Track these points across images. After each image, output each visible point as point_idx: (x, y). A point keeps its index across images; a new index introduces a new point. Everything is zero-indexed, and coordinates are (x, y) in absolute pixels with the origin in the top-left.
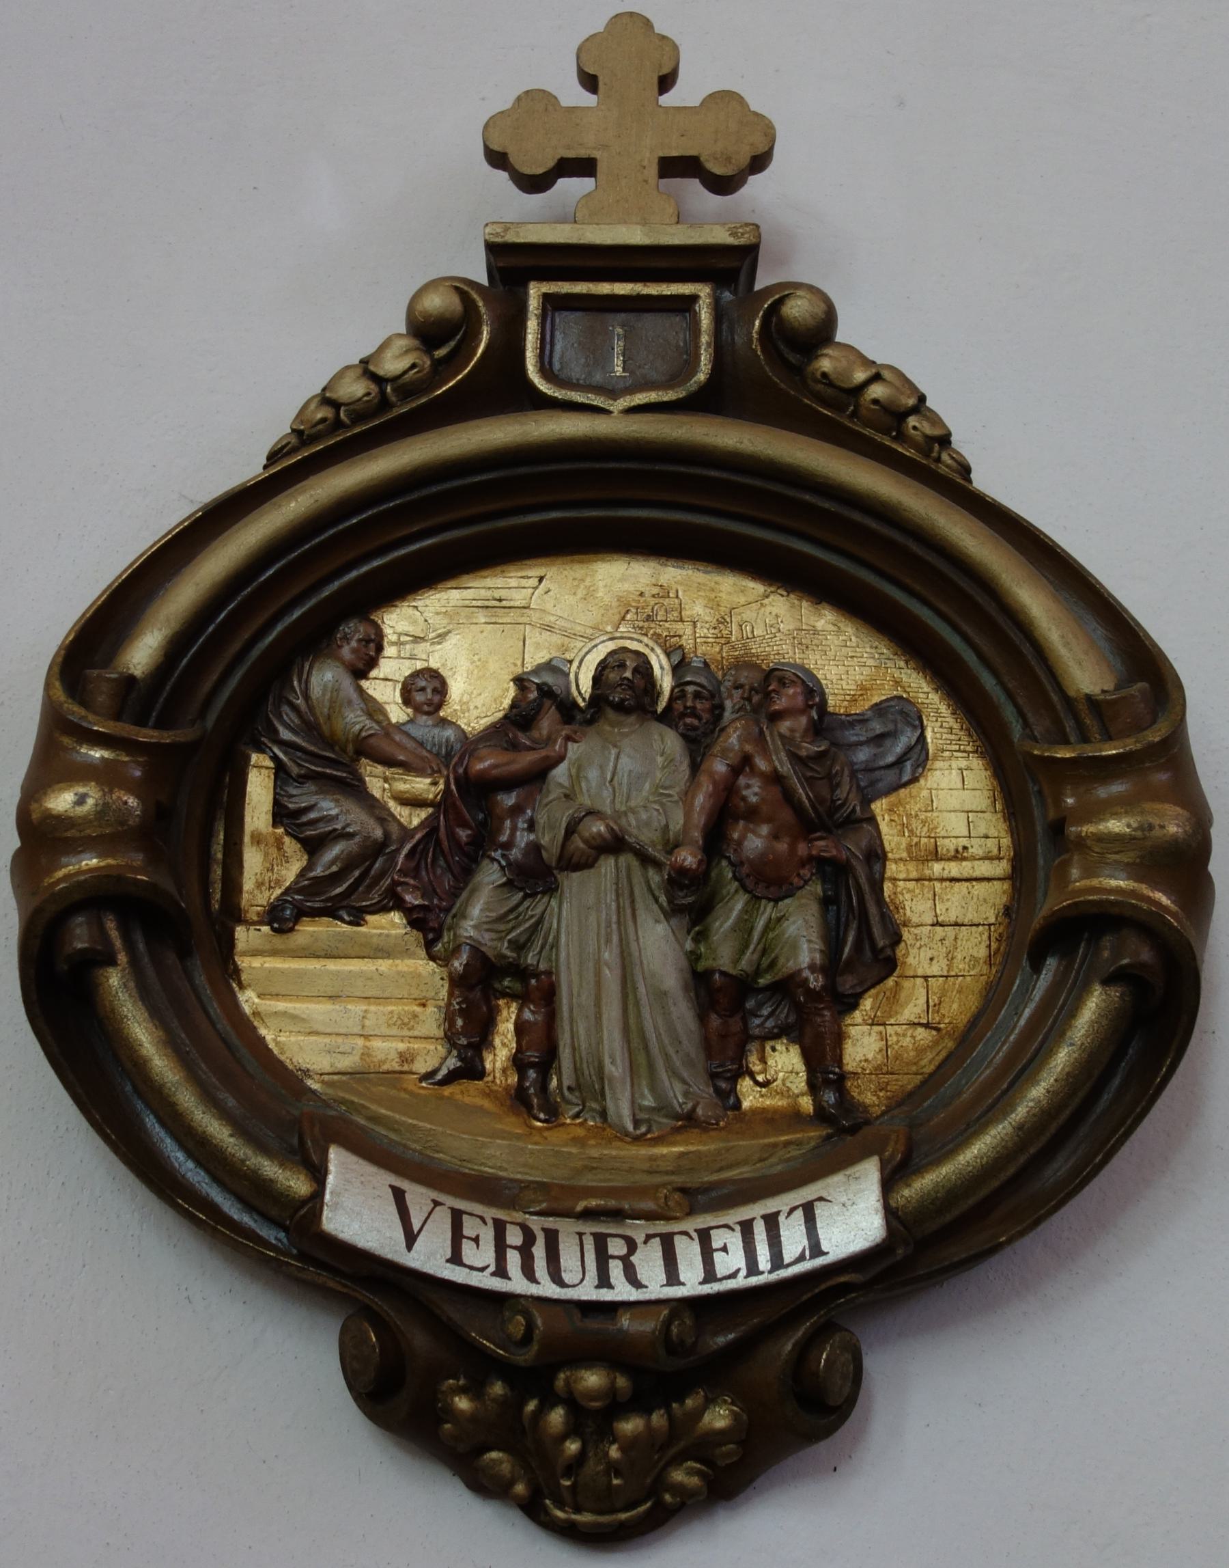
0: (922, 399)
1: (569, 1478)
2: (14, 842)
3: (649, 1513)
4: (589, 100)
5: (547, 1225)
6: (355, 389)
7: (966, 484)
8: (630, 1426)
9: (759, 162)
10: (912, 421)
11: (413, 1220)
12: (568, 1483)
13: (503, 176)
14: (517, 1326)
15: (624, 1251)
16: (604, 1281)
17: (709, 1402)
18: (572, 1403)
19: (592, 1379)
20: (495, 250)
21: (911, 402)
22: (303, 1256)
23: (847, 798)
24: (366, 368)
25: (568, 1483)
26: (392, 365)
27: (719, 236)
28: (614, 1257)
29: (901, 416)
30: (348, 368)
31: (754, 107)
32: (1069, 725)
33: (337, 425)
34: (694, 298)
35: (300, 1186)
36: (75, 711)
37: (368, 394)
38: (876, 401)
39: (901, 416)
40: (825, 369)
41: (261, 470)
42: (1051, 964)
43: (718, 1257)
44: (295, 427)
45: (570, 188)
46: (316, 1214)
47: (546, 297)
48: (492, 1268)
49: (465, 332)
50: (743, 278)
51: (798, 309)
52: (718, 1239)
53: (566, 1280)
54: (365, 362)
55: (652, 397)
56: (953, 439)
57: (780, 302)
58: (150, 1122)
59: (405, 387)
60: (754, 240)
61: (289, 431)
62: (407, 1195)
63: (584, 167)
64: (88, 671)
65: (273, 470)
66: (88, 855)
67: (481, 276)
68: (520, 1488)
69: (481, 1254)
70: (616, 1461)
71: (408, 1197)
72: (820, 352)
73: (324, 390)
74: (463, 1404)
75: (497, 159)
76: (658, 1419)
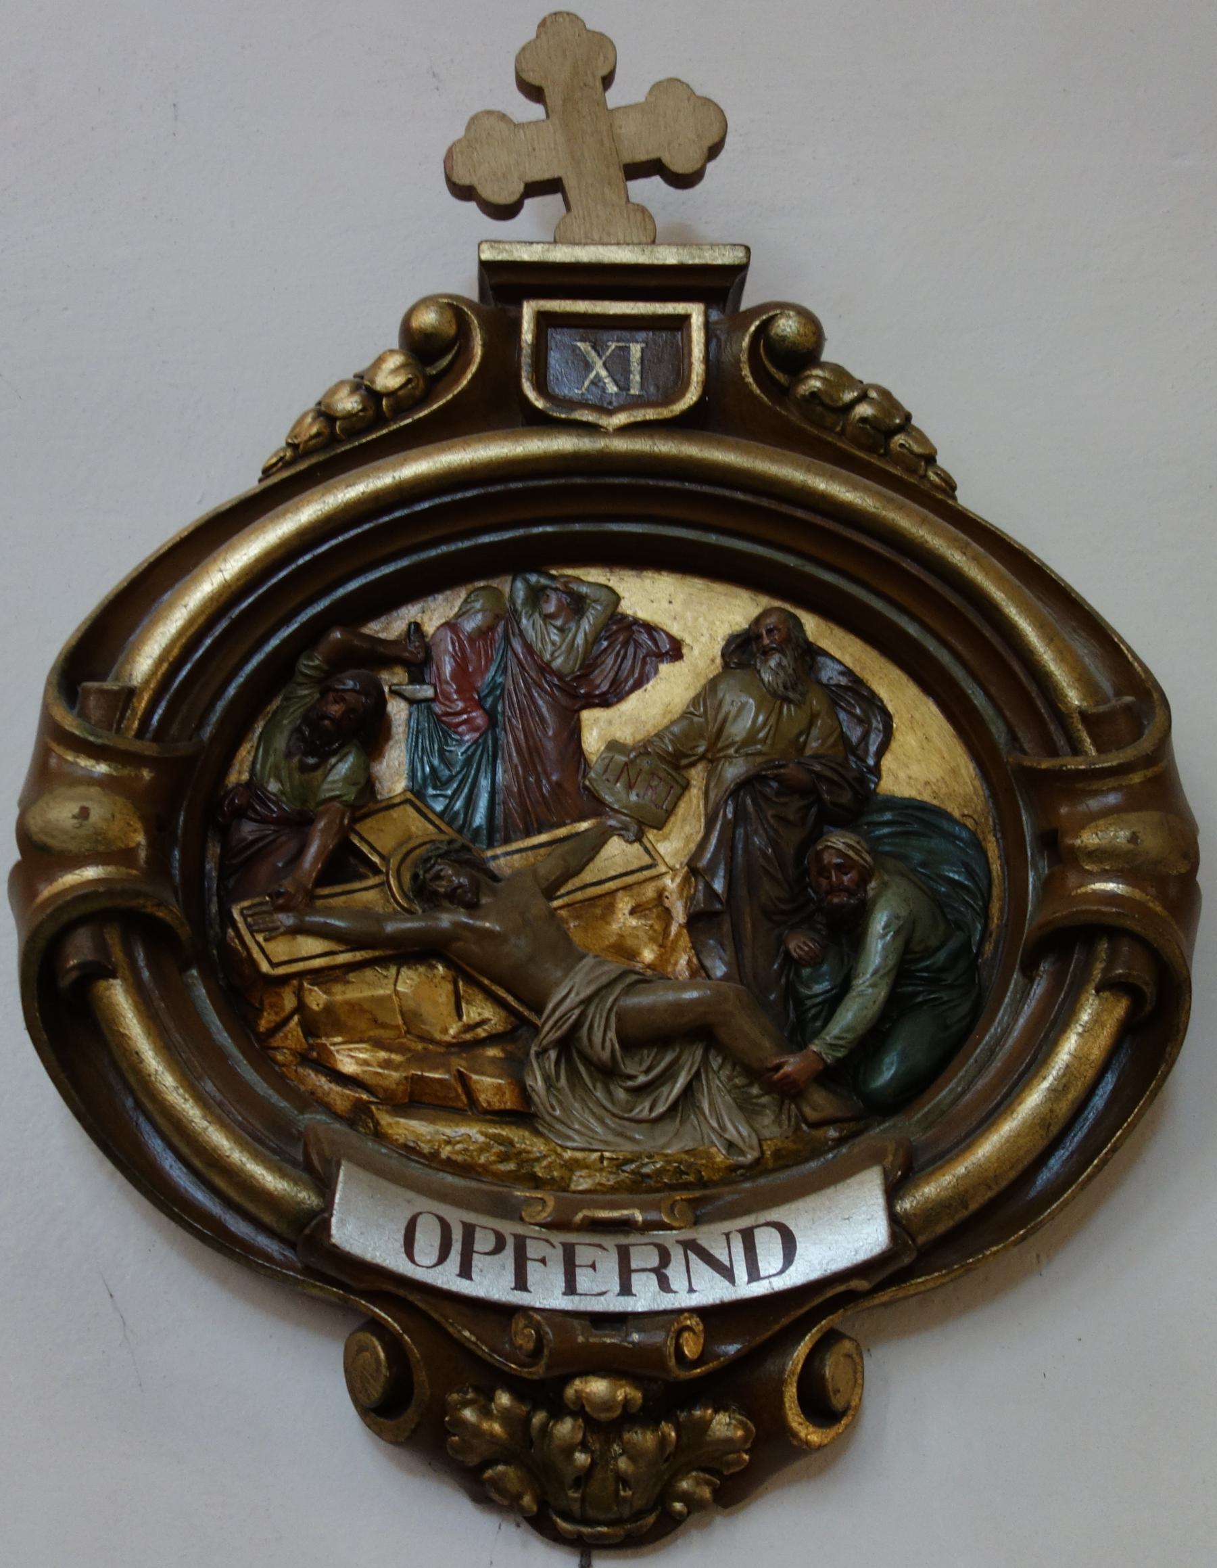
0: (908, 417)
2: (14, 855)
4: (535, 111)
6: (348, 403)
8: (644, 1439)
10: (900, 439)
14: (524, 1339)
15: (655, 1262)
17: (716, 1411)
18: (580, 1409)
19: (598, 1387)
20: (488, 268)
22: (308, 1271)
23: (600, 685)
24: (362, 385)
26: (389, 379)
30: (341, 383)
32: (1061, 742)
35: (306, 1197)
36: (69, 722)
38: (864, 420)
41: (256, 483)
42: (1044, 967)
44: (290, 441)
46: (326, 1225)
49: (459, 348)
50: (729, 304)
51: (787, 326)
53: (417, 1259)
54: (360, 376)
56: (938, 458)
59: (402, 401)
61: (283, 444)
67: (473, 294)
68: (527, 1500)
75: (464, 192)
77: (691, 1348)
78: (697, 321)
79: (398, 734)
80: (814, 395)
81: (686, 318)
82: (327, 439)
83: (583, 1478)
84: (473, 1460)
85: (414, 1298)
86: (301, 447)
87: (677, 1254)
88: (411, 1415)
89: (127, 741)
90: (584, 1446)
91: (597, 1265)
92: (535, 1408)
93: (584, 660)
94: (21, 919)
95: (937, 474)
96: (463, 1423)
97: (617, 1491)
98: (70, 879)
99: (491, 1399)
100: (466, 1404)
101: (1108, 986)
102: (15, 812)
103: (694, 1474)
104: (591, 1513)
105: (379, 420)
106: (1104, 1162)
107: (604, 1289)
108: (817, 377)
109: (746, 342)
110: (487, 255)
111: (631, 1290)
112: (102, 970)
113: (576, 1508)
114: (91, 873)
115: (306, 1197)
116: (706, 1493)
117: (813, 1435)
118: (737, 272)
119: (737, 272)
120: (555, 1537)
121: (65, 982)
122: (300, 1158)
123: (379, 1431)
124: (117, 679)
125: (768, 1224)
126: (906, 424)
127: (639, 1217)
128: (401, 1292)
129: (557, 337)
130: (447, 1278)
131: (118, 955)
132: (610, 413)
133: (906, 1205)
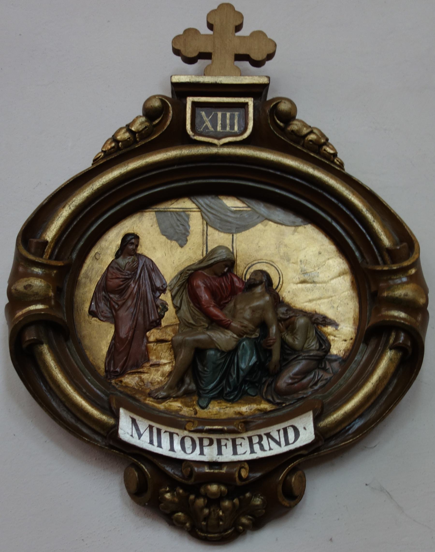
0: (327, 140)
2: (6, 301)
4: (211, 32)
6: (124, 136)
7: (342, 170)
8: (227, 503)
9: (270, 56)
10: (324, 147)
13: (179, 58)
18: (205, 496)
19: (214, 488)
21: (323, 141)
24: (128, 128)
27: (264, 80)
28: (238, 445)
29: (321, 145)
30: (121, 129)
35: (112, 421)
37: (129, 138)
38: (311, 141)
39: (321, 145)
41: (91, 165)
43: (238, 447)
45: (201, 63)
47: (194, 104)
51: (284, 107)
52: (238, 442)
57: (277, 104)
63: (207, 56)
64: (32, 239)
65: (95, 166)
67: (170, 95)
70: (221, 516)
71: (138, 422)
72: (291, 122)
73: (113, 136)
74: (168, 496)
75: (177, 52)
76: (236, 501)
77: (244, 473)
79: (37, 282)
82: (116, 149)
83: (206, 518)
84: (168, 512)
85: (144, 454)
86: (107, 152)
87: (265, 438)
88: (148, 495)
91: (243, 444)
92: (191, 493)
95: (338, 161)
97: (219, 523)
98: (33, 308)
101: (396, 347)
102: (7, 285)
105: (136, 142)
107: (245, 451)
108: (296, 125)
110: (176, 79)
111: (254, 451)
114: (40, 307)
115: (112, 421)
117: (286, 503)
119: (265, 87)
121: (25, 346)
125: (190, 437)
127: (225, 428)
129: (198, 110)
130: (155, 449)
132: (219, 139)
133: (323, 424)
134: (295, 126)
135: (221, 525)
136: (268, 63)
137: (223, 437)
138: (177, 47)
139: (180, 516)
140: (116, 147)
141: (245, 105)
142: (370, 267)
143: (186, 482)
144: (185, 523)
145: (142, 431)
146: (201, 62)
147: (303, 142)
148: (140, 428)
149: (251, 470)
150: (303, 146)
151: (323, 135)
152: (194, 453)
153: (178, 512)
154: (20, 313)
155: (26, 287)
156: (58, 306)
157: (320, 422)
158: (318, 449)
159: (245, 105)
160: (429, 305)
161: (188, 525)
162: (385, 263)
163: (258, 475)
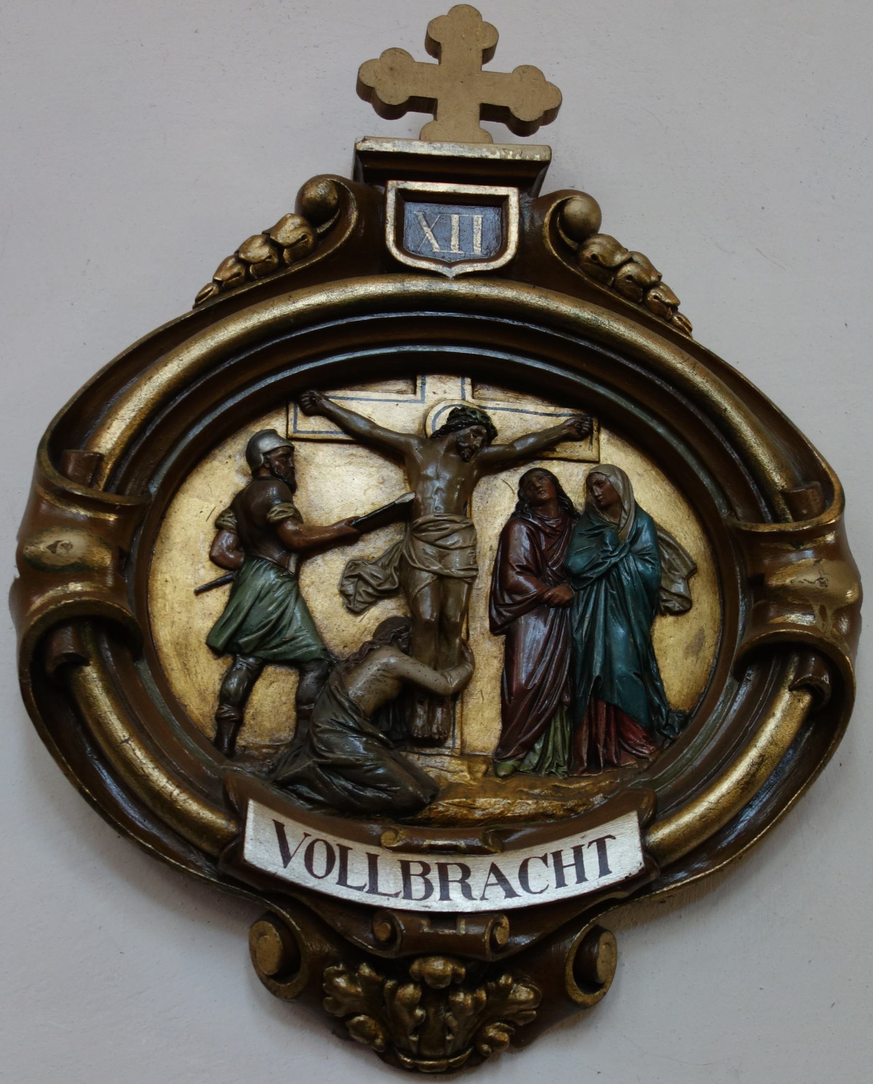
0: (660, 277)
1: (415, 1036)
2: (14, 573)
3: (471, 1055)
4: (435, 61)
5: (515, 899)
6: (260, 252)
9: (549, 116)
11: (290, 846)
12: (414, 1039)
13: (368, 107)
15: (459, 876)
16: (445, 896)
18: (420, 981)
19: (438, 965)
20: (362, 156)
21: (653, 278)
24: (268, 238)
25: (414, 1039)
26: (290, 233)
30: (253, 238)
31: (548, 79)
33: (249, 278)
34: (506, 198)
35: (232, 828)
38: (630, 277)
40: (595, 253)
41: (191, 309)
42: (751, 675)
48: (367, 888)
50: (535, 187)
51: (576, 208)
55: (469, 269)
58: (105, 774)
59: (298, 250)
60: (547, 158)
61: (211, 281)
62: (285, 828)
63: (426, 105)
66: (389, 653)
69: (358, 875)
71: (287, 830)
73: (238, 252)
75: (366, 92)
78: (514, 201)
80: (594, 257)
81: (506, 198)
83: (420, 1027)
84: (340, 1013)
85: (304, 899)
89: (98, 491)
90: (422, 1004)
93: (592, 438)
94: (19, 627)
96: (337, 988)
99: (357, 970)
100: (339, 974)
102: (14, 544)
103: (498, 1024)
104: (427, 1053)
106: (793, 805)
109: (547, 220)
110: (362, 147)
112: (79, 661)
113: (414, 1049)
115: (232, 828)
116: (505, 1037)
117: (580, 997)
118: (544, 165)
120: (398, 1066)
121: (50, 668)
122: (220, 795)
123: (274, 992)
124: (85, 449)
126: (656, 285)
128: (294, 895)
129: (413, 210)
130: (330, 886)
131: (90, 647)
132: (450, 265)
134: (595, 248)
135: (449, 1041)
136: (542, 129)
137: (450, 862)
138: (370, 82)
139: (362, 1022)
140: (243, 274)
141: (501, 202)
142: (746, 526)
143: (379, 953)
144: (376, 1037)
145: (292, 848)
146: (410, 116)
147: (613, 279)
148: (289, 839)
149: (515, 930)
150: (614, 287)
151: (650, 268)
152: (432, 898)
153: (359, 1015)
154: (38, 602)
155: (53, 548)
156: (118, 589)
157: (650, 834)
158: (648, 889)
159: (501, 202)
160: (863, 604)
161: (379, 1041)
162: (778, 518)
163: (523, 940)
